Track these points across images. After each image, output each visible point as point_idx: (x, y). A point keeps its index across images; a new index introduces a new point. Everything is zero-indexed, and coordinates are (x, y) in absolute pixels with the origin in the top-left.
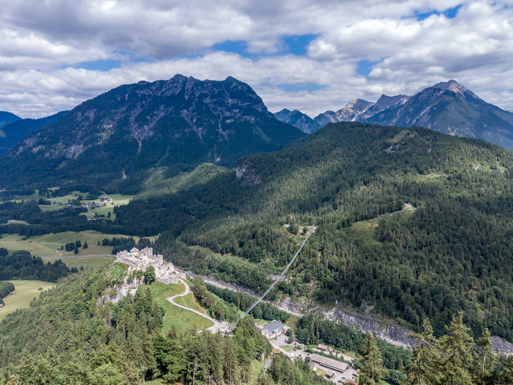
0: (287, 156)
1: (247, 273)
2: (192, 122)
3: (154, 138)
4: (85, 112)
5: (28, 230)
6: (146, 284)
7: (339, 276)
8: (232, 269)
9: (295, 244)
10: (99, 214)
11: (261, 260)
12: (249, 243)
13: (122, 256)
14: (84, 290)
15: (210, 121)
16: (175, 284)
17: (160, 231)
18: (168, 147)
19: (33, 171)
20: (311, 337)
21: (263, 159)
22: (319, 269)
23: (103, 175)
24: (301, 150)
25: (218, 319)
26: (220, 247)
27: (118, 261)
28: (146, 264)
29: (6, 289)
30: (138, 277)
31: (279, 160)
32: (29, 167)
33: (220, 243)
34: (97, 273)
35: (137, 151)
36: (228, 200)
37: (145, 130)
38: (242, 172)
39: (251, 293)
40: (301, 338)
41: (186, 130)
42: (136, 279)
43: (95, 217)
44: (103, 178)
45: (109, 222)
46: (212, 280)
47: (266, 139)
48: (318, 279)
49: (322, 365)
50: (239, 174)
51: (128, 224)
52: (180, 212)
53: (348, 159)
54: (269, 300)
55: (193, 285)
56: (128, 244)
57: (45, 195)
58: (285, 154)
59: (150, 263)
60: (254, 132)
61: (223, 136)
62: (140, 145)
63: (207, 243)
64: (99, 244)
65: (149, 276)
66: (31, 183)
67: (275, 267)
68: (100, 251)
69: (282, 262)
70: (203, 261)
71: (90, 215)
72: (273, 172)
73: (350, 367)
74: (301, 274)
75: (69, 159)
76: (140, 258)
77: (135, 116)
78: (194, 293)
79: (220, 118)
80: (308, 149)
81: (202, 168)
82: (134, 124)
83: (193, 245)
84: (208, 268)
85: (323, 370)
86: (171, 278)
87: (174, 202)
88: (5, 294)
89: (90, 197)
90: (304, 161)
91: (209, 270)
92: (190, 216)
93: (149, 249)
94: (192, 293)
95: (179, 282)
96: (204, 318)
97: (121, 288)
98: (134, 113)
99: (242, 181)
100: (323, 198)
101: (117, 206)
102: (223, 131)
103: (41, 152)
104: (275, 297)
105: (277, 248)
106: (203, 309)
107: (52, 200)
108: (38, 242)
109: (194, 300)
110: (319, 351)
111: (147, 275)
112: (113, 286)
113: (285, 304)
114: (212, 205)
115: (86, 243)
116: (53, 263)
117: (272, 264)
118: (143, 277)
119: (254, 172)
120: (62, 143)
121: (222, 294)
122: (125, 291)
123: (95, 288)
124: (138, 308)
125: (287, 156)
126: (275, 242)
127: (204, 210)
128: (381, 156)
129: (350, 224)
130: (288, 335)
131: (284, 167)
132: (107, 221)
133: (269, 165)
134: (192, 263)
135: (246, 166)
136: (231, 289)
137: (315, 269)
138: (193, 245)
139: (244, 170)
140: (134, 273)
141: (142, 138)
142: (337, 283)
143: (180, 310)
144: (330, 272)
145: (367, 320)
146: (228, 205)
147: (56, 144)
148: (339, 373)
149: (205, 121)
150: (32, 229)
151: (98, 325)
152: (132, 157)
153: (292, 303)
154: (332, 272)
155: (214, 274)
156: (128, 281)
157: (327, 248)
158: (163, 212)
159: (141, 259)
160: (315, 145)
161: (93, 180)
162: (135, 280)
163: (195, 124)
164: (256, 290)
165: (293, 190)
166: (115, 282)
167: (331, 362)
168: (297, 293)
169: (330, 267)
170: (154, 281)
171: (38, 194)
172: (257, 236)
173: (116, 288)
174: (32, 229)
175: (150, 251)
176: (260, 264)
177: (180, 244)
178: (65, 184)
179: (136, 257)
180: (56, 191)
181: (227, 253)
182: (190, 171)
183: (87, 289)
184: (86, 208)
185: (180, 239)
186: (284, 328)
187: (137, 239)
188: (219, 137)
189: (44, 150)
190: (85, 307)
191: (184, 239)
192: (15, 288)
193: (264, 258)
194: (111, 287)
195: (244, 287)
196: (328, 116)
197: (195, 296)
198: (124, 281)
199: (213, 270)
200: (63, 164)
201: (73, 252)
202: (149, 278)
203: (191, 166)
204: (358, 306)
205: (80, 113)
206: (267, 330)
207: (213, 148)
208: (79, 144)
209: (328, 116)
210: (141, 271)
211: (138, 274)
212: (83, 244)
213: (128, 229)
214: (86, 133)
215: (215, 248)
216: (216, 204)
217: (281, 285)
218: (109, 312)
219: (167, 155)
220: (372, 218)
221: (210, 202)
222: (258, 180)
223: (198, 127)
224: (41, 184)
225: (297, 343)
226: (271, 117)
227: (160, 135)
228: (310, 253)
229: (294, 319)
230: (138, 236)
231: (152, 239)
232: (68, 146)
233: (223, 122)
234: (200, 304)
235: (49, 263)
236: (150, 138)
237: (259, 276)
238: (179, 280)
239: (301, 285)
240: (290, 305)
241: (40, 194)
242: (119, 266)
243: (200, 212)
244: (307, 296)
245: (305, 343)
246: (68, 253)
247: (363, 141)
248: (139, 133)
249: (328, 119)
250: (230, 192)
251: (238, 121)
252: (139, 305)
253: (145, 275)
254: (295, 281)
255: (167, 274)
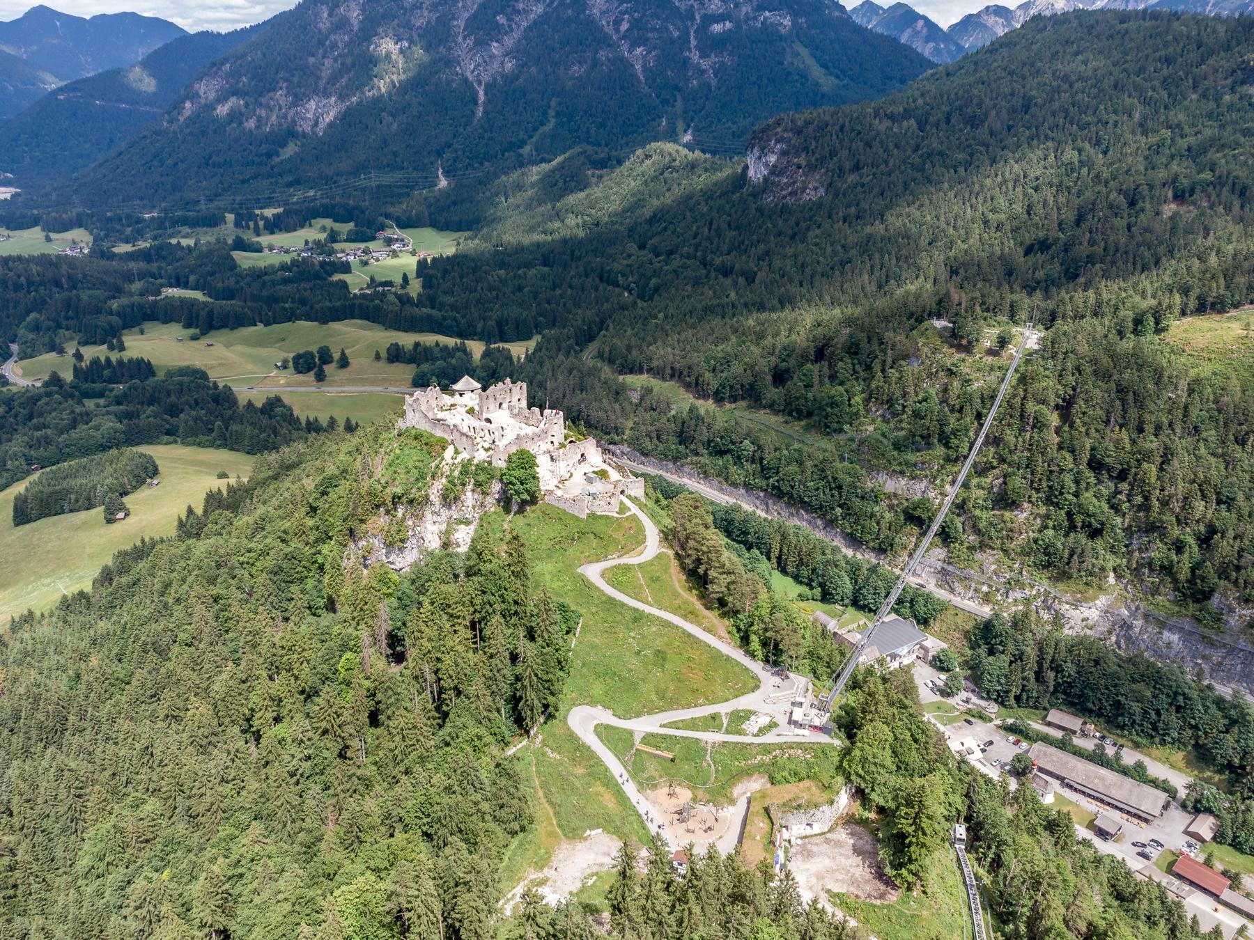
0: (907, 114)
1: (800, 463)
2: (617, 31)
3: (518, 78)
4: (337, 6)
5: (203, 314)
6: (507, 510)
7: (1128, 495)
8: (752, 448)
9: (968, 382)
10: (379, 279)
11: (847, 427)
12: (804, 375)
13: (424, 407)
14: (311, 507)
15: (667, 29)
16: (607, 517)
17: (538, 328)
18: (553, 104)
19: (219, 166)
20: (1024, 686)
21: (834, 125)
22: (1056, 469)
23: (388, 178)
24: (953, 96)
25: (776, 664)
26: (714, 383)
27: (409, 424)
28: (505, 441)
29: (136, 472)
30: (478, 484)
31: (882, 126)
32: (211, 157)
33: (714, 371)
34: (349, 453)
35: (473, 113)
36: (725, 248)
37: (492, 57)
38: (766, 165)
39: (810, 523)
40: (986, 685)
41: (602, 54)
42: (473, 491)
43: (369, 287)
44: (390, 186)
45: (404, 300)
46: (690, 476)
47: (821, 81)
48: (1048, 501)
49: (1071, 787)
50: (757, 172)
51: (453, 307)
52: (590, 280)
53: (1113, 118)
54: (873, 549)
55: (667, 521)
56: (454, 361)
57: (249, 228)
58: (901, 109)
59: (518, 437)
60: (788, 59)
61: (703, 72)
62: (482, 97)
63: (672, 368)
64: (378, 357)
65: (518, 486)
66: (217, 195)
67: (895, 453)
68: (380, 377)
69: (918, 439)
70: (664, 420)
71: (356, 281)
72: (861, 164)
73: (1174, 804)
74: (988, 480)
75: (304, 135)
76: (485, 415)
77: (466, 15)
78: (677, 555)
79: (693, 18)
80: (976, 92)
81: (648, 156)
82: (464, 38)
83: (631, 371)
84: (676, 440)
85: (1078, 806)
86: (593, 496)
87: (573, 252)
88: (134, 483)
89: (357, 233)
90: (961, 130)
91: (681, 448)
92: (617, 290)
93: (516, 389)
94: (671, 553)
95: (623, 509)
96: (717, 656)
97: (420, 518)
98: (464, 6)
99: (764, 191)
100: (1028, 242)
101: (425, 260)
102: (701, 57)
103: (235, 116)
104: (892, 545)
105: (905, 395)
106: (712, 616)
107: (265, 240)
108: (228, 346)
109: (677, 579)
110: (1058, 734)
111: (511, 483)
112: (395, 510)
113: (927, 569)
114: (676, 262)
115: (343, 353)
116: (259, 405)
117: (885, 441)
118: (496, 487)
119: (804, 163)
120: (285, 91)
121: (722, 519)
122: (436, 528)
123: (340, 512)
124: (477, 601)
125: (907, 114)
126: (897, 375)
127: (656, 273)
128: (1230, 107)
129: (1164, 323)
130: (942, 669)
131: (897, 146)
132: (399, 297)
133: (852, 140)
134: (630, 424)
135: (779, 146)
136: (749, 506)
137: (1041, 466)
138: (631, 373)
139: (772, 159)
140: (464, 472)
141: (486, 78)
142: (1119, 520)
143: (628, 616)
144: (1093, 480)
145: (1232, 651)
146: (723, 262)
147: (271, 94)
148: (1136, 821)
149: (654, 29)
150: (211, 311)
151: (345, 647)
152: (461, 130)
153: (950, 568)
154: (1100, 482)
155: (695, 458)
156: (444, 497)
157: (1086, 401)
158: (543, 278)
159: (489, 421)
160: (999, 79)
161: (364, 189)
162: (469, 494)
163: (624, 37)
164: (828, 517)
165: (928, 217)
166: (399, 498)
167: (1103, 779)
168: (972, 538)
169: (1096, 465)
170: (533, 500)
171: (231, 225)
172: (833, 353)
173: (403, 520)
174: (211, 311)
175: (518, 394)
176: (841, 438)
177: (595, 368)
178: (295, 199)
179: (471, 411)
180: (277, 216)
181: (735, 401)
182: (612, 168)
183: (320, 504)
184: (348, 263)
185: (595, 353)
186: (928, 644)
187: (477, 348)
188: (690, 74)
189: (244, 110)
190: (314, 563)
191: (606, 355)
192: (160, 468)
193: (856, 423)
194: (388, 512)
195: (789, 505)
196: (991, 20)
197: (683, 567)
198: (432, 497)
199: (692, 447)
200: (290, 150)
201: (311, 377)
202: (518, 493)
203: (614, 153)
204: (1197, 601)
205: (324, 7)
206: (875, 648)
207: (673, 106)
208: (327, 94)
209: (991, 20)
210: (490, 463)
211: (479, 475)
212: (336, 356)
213: (455, 319)
214: (343, 64)
215: (697, 384)
216: (688, 258)
217: (915, 509)
218: (380, 606)
219: (551, 125)
220: (1236, 306)
221: (670, 253)
222: (816, 189)
223: (633, 45)
224: (238, 198)
225: (974, 699)
226: (837, 14)
227: (533, 70)
228: (1022, 416)
229: (959, 620)
230: (480, 340)
231: (519, 350)
232: (299, 99)
233: (703, 28)
234: (702, 597)
235: (250, 404)
236: (510, 79)
237: (841, 476)
238: (621, 503)
239: (985, 516)
240: (944, 572)
241: (237, 224)
242: (414, 443)
243: (643, 280)
244: (1005, 551)
245: (1001, 699)
246: (301, 377)
247: (1168, 61)
248: (479, 65)
249: (984, 27)
250: (729, 226)
251: (745, 27)
252: (484, 592)
253: (501, 480)
254: (964, 502)
255: (578, 477)
